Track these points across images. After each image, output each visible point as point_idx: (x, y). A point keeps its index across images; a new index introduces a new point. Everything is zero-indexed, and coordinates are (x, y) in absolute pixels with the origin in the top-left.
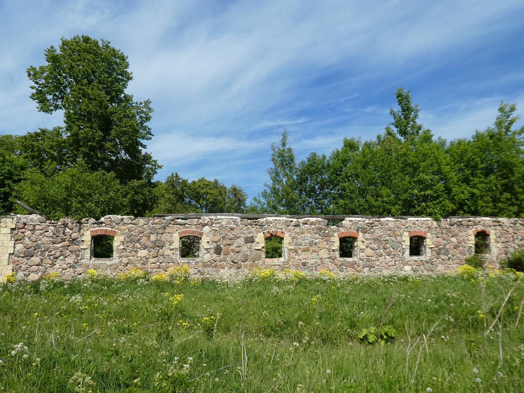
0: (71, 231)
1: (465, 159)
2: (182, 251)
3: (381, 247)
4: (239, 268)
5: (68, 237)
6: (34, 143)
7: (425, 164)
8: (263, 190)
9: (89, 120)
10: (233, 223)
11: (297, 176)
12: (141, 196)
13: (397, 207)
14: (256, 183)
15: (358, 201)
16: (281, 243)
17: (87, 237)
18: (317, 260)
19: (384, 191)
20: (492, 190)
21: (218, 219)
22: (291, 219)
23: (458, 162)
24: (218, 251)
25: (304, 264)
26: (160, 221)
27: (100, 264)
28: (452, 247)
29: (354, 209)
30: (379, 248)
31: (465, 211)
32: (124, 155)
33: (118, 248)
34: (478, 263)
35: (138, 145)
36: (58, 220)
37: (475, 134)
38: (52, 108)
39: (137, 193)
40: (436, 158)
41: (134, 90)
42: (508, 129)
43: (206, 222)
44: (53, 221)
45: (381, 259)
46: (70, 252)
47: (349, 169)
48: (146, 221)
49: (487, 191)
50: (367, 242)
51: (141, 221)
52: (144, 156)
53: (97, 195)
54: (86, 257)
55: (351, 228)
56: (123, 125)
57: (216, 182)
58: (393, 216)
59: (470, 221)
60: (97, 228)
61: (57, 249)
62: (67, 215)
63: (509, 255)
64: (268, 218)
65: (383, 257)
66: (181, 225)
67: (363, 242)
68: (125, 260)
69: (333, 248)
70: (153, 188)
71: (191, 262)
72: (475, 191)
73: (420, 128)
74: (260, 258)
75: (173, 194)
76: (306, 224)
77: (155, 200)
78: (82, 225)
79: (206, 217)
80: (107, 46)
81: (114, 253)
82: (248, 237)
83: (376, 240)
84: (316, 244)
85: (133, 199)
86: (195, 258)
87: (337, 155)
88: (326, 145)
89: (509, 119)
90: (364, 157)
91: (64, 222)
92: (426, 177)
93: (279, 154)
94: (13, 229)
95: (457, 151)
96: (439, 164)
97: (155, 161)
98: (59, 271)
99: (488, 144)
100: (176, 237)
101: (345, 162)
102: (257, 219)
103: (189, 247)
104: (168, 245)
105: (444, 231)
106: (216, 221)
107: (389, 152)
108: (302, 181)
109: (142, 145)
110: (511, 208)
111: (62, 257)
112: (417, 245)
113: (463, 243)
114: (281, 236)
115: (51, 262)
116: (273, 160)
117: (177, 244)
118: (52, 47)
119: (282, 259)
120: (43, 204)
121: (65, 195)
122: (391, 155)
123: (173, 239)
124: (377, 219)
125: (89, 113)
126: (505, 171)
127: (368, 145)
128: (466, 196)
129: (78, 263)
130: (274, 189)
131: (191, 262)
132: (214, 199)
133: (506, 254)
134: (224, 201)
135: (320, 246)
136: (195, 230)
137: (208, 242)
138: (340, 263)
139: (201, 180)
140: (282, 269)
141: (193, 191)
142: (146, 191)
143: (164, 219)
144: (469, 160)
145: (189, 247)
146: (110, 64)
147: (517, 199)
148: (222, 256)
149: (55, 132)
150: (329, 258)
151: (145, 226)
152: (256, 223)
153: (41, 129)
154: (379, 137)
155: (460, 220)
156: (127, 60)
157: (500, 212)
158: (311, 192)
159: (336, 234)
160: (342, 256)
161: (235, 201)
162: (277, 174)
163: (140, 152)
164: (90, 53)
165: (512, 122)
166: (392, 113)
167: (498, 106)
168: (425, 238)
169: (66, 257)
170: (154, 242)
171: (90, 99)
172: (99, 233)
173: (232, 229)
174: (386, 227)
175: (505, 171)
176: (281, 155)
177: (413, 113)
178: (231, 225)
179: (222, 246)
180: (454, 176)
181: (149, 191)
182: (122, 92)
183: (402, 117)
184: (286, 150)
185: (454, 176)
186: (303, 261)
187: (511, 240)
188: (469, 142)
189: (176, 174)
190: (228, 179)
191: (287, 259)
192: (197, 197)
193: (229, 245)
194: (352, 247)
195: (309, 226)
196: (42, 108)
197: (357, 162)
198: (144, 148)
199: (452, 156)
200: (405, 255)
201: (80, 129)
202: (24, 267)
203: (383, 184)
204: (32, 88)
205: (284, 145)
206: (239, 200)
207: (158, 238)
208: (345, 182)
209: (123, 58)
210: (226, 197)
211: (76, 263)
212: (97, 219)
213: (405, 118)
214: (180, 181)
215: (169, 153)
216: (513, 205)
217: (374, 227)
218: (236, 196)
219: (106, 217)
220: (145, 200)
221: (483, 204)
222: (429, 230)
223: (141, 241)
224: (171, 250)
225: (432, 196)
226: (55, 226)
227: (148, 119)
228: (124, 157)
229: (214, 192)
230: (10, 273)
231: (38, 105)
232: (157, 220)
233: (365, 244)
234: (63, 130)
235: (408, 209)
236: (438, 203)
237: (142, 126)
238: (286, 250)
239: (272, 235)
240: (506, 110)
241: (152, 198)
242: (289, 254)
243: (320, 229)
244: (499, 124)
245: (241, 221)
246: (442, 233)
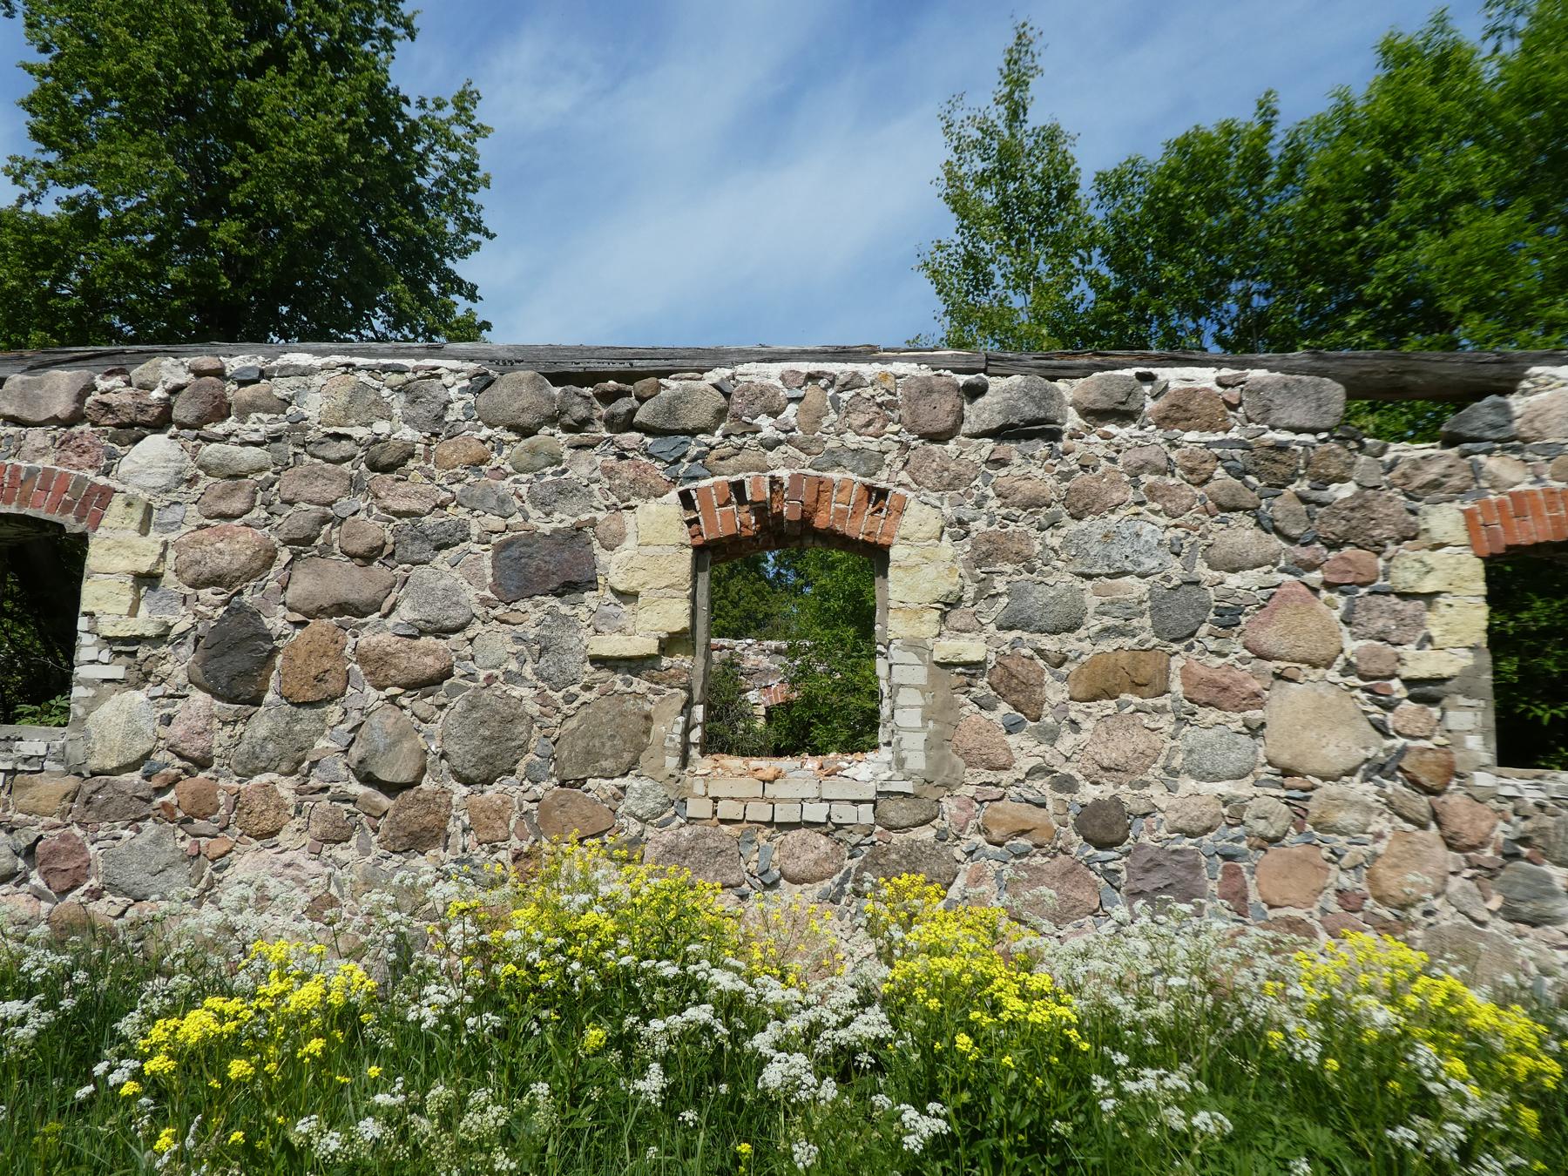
10: (398, 403)
18: (1244, 789)
24: (236, 663)
69: (1423, 664)
84: (1228, 618)
114: (860, 527)
119: (866, 771)
135: (1269, 638)
138: (1502, 832)
150: (1378, 769)
159: (1444, 520)
176: (1006, 164)
178: (382, 427)
179: (276, 621)
186: (1089, 793)
191: (917, 761)
195: (1157, 436)
242: (940, 714)
243: (1272, 466)
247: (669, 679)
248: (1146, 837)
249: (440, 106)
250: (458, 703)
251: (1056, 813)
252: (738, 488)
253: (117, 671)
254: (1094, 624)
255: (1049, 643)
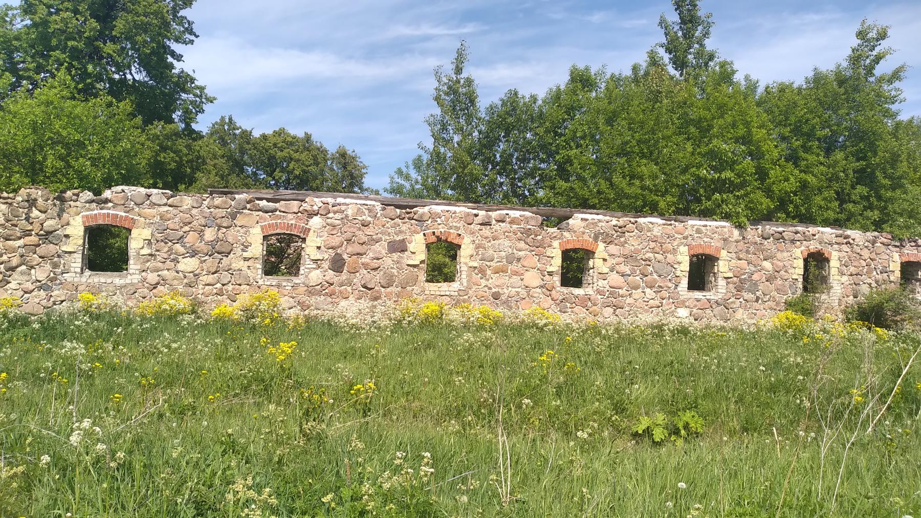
0: (43, 216)
1: (793, 119)
2: (266, 262)
3: (638, 272)
5: (36, 227)
7: (721, 121)
8: (414, 156)
10: (367, 212)
11: (480, 132)
12: (172, 155)
13: (669, 198)
14: (394, 144)
16: (454, 257)
17: (76, 229)
18: (519, 290)
19: (646, 168)
20: (838, 179)
21: (339, 204)
22: (475, 212)
24: (337, 264)
25: (496, 296)
26: (226, 202)
27: (100, 284)
28: (764, 279)
29: (588, 199)
30: (633, 273)
31: (788, 214)
32: (137, 74)
33: (138, 254)
35: (165, 52)
36: (15, 191)
37: (810, 74)
39: (164, 149)
40: (742, 113)
42: (870, 71)
43: (315, 208)
45: (637, 294)
46: (40, 257)
47: (577, 124)
48: (197, 201)
50: (611, 261)
51: (187, 200)
52: (179, 76)
53: (96, 146)
54: (72, 269)
55: (584, 233)
56: (140, 10)
57: (308, 138)
58: (661, 215)
59: (796, 233)
60: (96, 212)
61: (14, 250)
62: (33, 182)
63: (861, 299)
64: (433, 207)
65: (640, 290)
66: (267, 212)
67: (605, 260)
68: (152, 278)
69: (550, 269)
70: (195, 140)
71: (284, 284)
72: (810, 178)
73: (711, 57)
74: (415, 281)
75: (223, 157)
76: (503, 222)
77: (198, 164)
78: (67, 204)
79: (315, 199)
81: (131, 262)
82: (395, 241)
83: (628, 258)
84: (519, 260)
85: (156, 160)
86: (292, 278)
87: (556, 97)
89: (874, 53)
90: (610, 103)
91: (29, 195)
93: (450, 88)
95: (779, 103)
96: (747, 124)
97: (202, 89)
99: (836, 95)
100: (256, 237)
101: (571, 110)
102: (412, 207)
103: (281, 256)
104: (239, 249)
105: (752, 249)
106: (335, 208)
107: (656, 97)
108: (489, 142)
109: (173, 53)
110: (869, 213)
111: (24, 267)
112: (701, 272)
113: (782, 273)
114: (456, 242)
117: (257, 249)
119: (455, 286)
121: (30, 142)
122: (661, 102)
123: (249, 239)
124: (632, 220)
126: (862, 145)
127: (616, 80)
128: (792, 185)
129: (56, 279)
130: (438, 154)
131: (284, 284)
132: (304, 171)
133: (855, 297)
134: (322, 175)
135: (525, 264)
136: (293, 222)
137: (319, 248)
138: (561, 298)
139: (280, 133)
140: (457, 300)
141: (261, 153)
142: (181, 144)
143: (233, 199)
144: (800, 121)
145: (281, 256)
147: (879, 198)
148: (344, 276)
150: (542, 287)
151: (194, 211)
152: (411, 215)
154: (635, 69)
155: (781, 229)
157: (848, 220)
158: (504, 167)
159: (556, 244)
160: (565, 282)
161: (343, 176)
162: (444, 128)
163: (172, 66)
165: (878, 59)
166: (663, 23)
167: (857, 27)
168: (718, 259)
169: (32, 267)
170: (212, 244)
172: (101, 222)
173: (365, 225)
174: (649, 234)
175: (862, 145)
176: (452, 90)
177: (700, 28)
178: (364, 217)
179: (345, 256)
180: (773, 150)
181: (188, 147)
183: (680, 34)
184: (462, 81)
185: (773, 150)
186: (494, 290)
187: (865, 270)
188: (800, 89)
189: (230, 119)
190: (330, 137)
191: (465, 284)
192: (270, 165)
193: (358, 254)
195: (508, 226)
197: (598, 112)
198: (179, 61)
199: (769, 111)
200: (679, 289)
201: (51, 14)
203: (643, 156)
205: (458, 70)
206: (352, 176)
207: (220, 235)
208: (571, 148)
210: (326, 169)
211: (52, 280)
212: (97, 193)
213: (684, 35)
214: (237, 132)
216: (871, 207)
217: (627, 234)
218: (345, 167)
219: (114, 189)
220: (180, 164)
221: (822, 203)
222: (725, 245)
223: (186, 240)
224: (246, 259)
225: (731, 182)
226: (11, 204)
228: (137, 77)
229: (303, 156)
232: (218, 200)
234: (15, 12)
235: (689, 203)
236: (742, 197)
237: (175, 16)
238: (464, 268)
242: (469, 276)
243: (528, 232)
244: (855, 59)
245: (384, 209)
246: (748, 252)
247: (421, 269)
248: (503, 298)
250: (382, 273)
251: (488, 293)
252: (434, 233)
253: (314, 266)
254: (496, 260)
255: (488, 263)
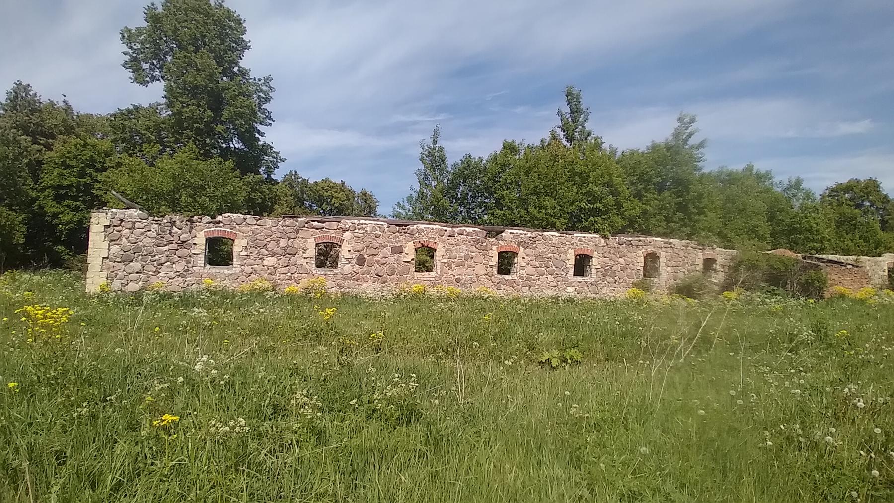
0: (180, 232)
4: (384, 282)
5: (176, 239)
6: (126, 122)
9: (194, 96)
15: (850, 389)
17: (200, 240)
19: (549, 202)
20: (665, 208)
23: (629, 175)
24: (361, 261)
25: (458, 280)
31: (635, 230)
32: (237, 144)
34: (646, 288)
36: (163, 216)
37: (650, 144)
38: (148, 79)
40: (607, 168)
41: (251, 64)
42: (685, 141)
44: (156, 219)
49: (661, 209)
51: (268, 222)
57: (343, 183)
58: (558, 231)
63: (679, 281)
68: (248, 269)
72: (648, 207)
77: (275, 199)
80: (221, 6)
81: (235, 260)
87: (495, 158)
88: (483, 147)
89: (688, 131)
92: (595, 188)
93: (429, 153)
94: (106, 227)
96: (610, 175)
97: (277, 153)
98: (166, 280)
100: (311, 244)
101: (503, 167)
102: (406, 226)
103: (327, 256)
105: (612, 251)
108: (454, 185)
110: (684, 229)
112: (581, 264)
115: (155, 269)
116: (421, 160)
117: (312, 252)
118: (153, 5)
119: (433, 274)
120: (144, 197)
125: (196, 87)
127: (531, 148)
139: (325, 181)
140: (434, 283)
142: (265, 188)
145: (327, 256)
146: (223, 27)
147: (690, 220)
148: (365, 268)
149: (151, 110)
151: (273, 229)
153: (134, 106)
156: (244, 25)
159: (494, 248)
162: (426, 177)
164: (200, 13)
166: (559, 113)
167: (677, 116)
171: (198, 70)
176: (431, 155)
182: (237, 64)
183: (570, 120)
185: (626, 191)
188: (643, 153)
194: (510, 264)
196: (136, 79)
199: (623, 167)
202: (120, 274)
204: (125, 53)
205: (435, 142)
209: (239, 22)
211: (186, 271)
212: (213, 217)
215: (294, 143)
216: (685, 226)
220: (264, 200)
227: (268, 100)
228: (237, 146)
229: (340, 195)
230: (103, 281)
231: (131, 75)
232: (288, 222)
233: (526, 260)
235: (575, 223)
239: (423, 245)
240: (685, 121)
241: (271, 198)
243: (477, 241)
244: (677, 135)
249: (260, 80)
251: (453, 279)
